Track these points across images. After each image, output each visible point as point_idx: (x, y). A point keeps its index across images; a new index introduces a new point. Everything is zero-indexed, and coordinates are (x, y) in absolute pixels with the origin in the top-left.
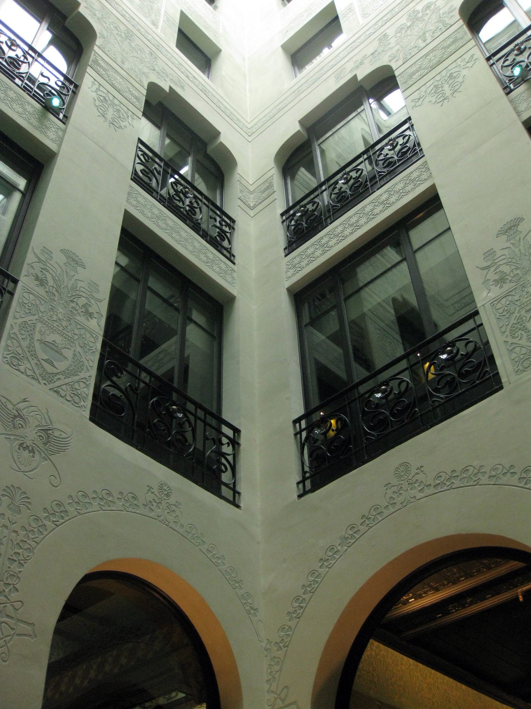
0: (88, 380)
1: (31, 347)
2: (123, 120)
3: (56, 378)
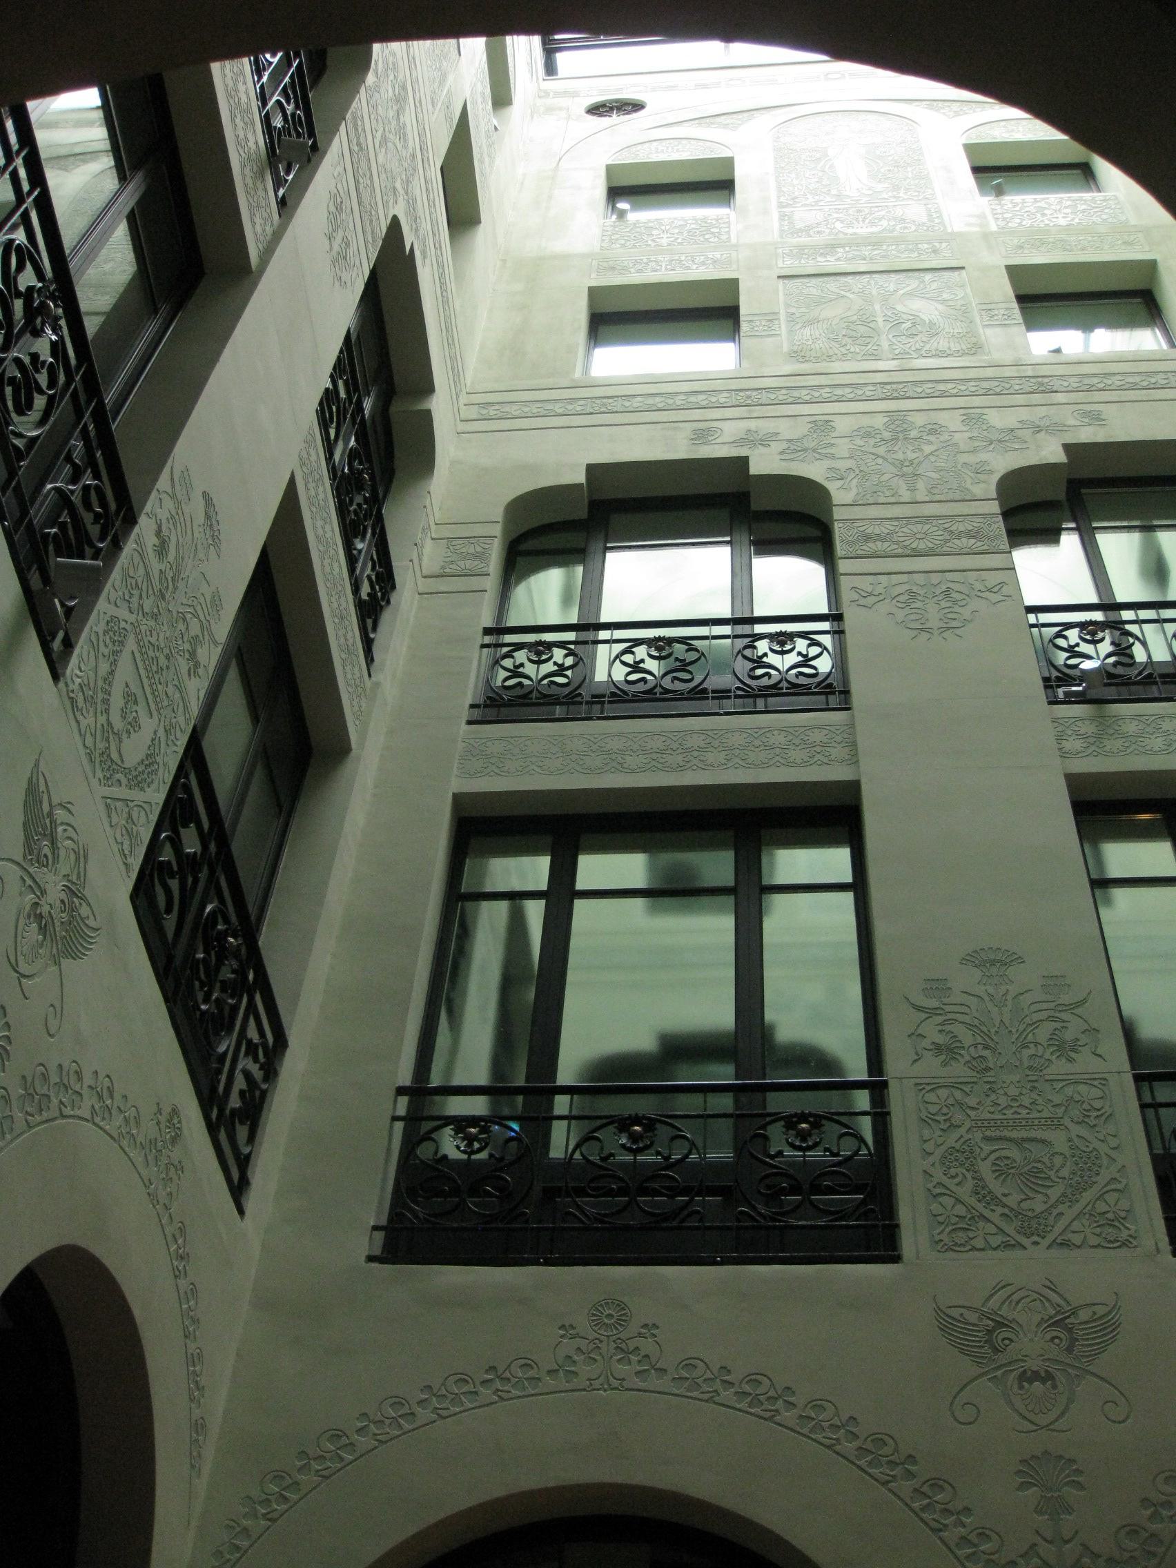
0: (1120, 1180)
1: (981, 1191)
2: (963, 603)
3: (1052, 1218)
